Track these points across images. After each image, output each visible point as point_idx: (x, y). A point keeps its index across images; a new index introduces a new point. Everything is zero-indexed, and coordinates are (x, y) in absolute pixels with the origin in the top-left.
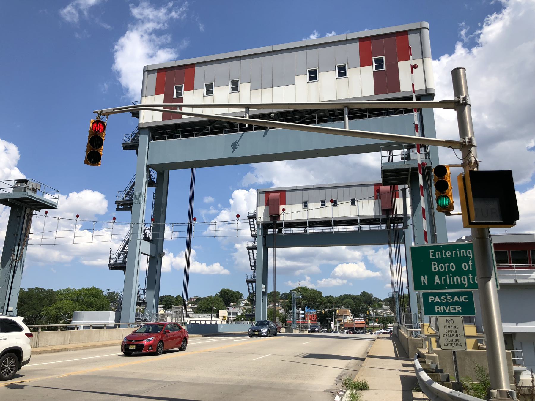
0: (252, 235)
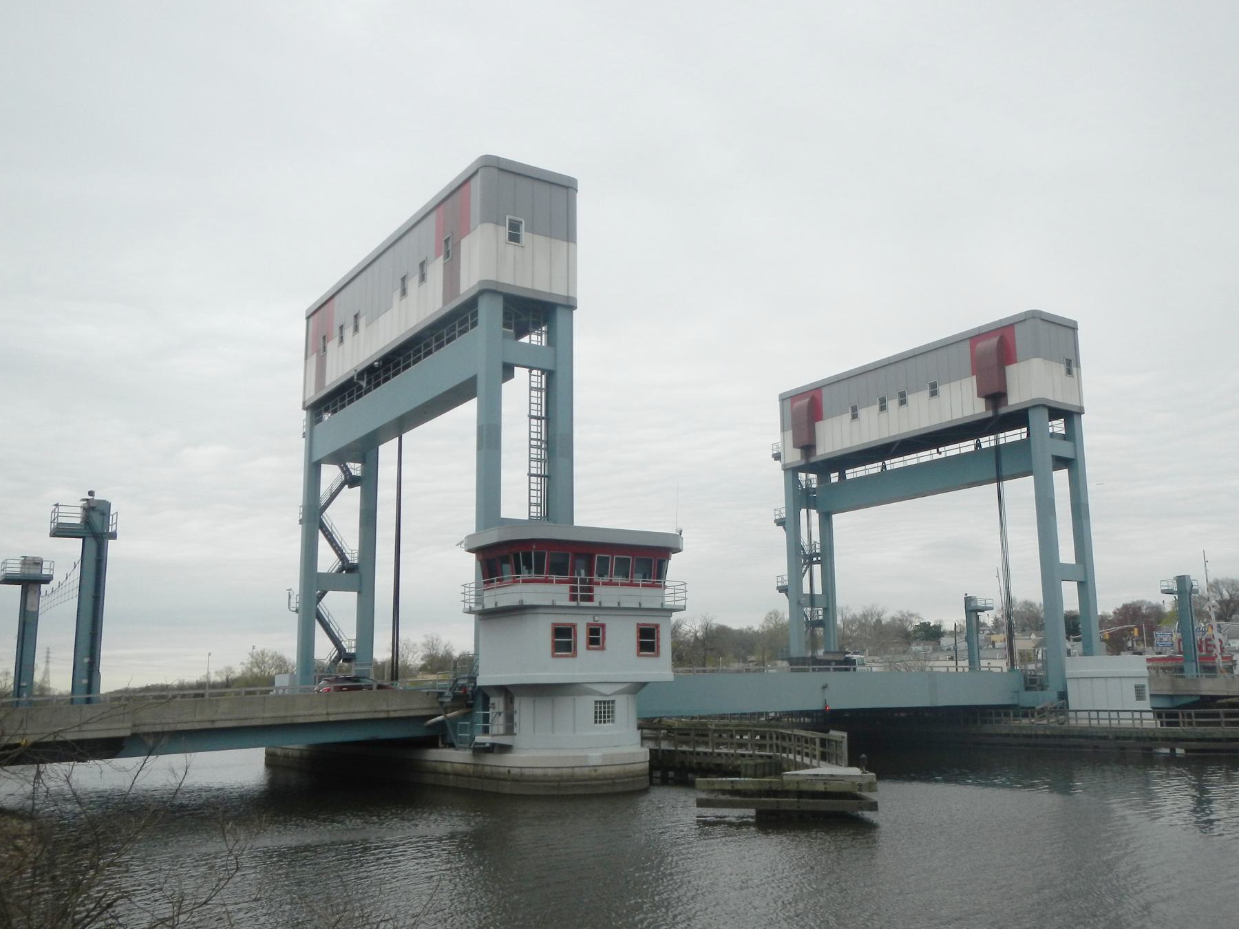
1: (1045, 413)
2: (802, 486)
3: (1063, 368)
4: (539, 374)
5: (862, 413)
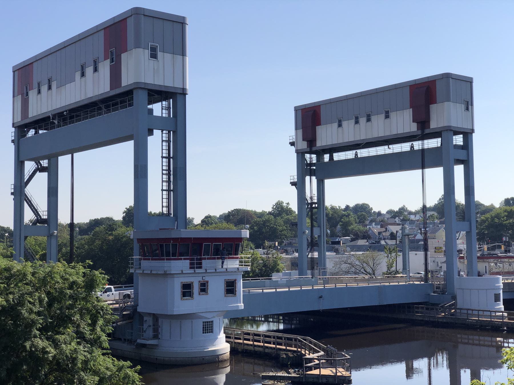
1: (452, 133)
2: (307, 162)
3: (463, 106)
4: (167, 133)
5: (345, 124)
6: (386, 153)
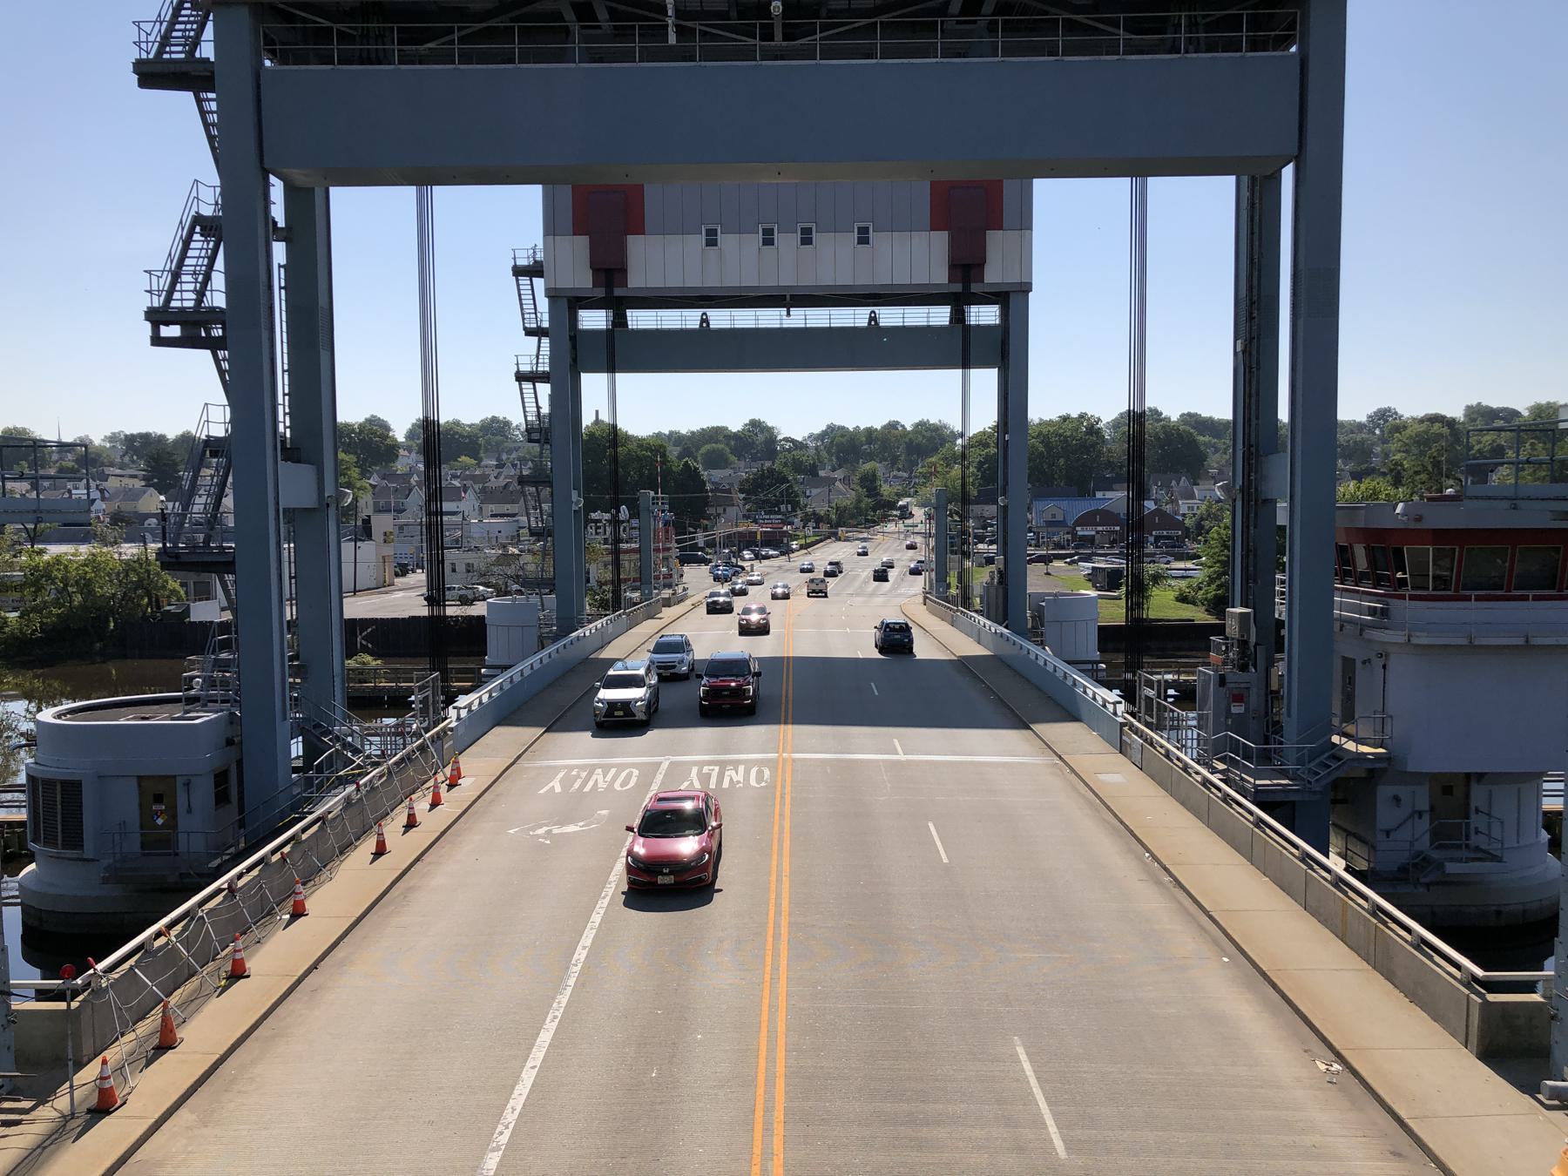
0: (525, 329)
6: (760, 326)
